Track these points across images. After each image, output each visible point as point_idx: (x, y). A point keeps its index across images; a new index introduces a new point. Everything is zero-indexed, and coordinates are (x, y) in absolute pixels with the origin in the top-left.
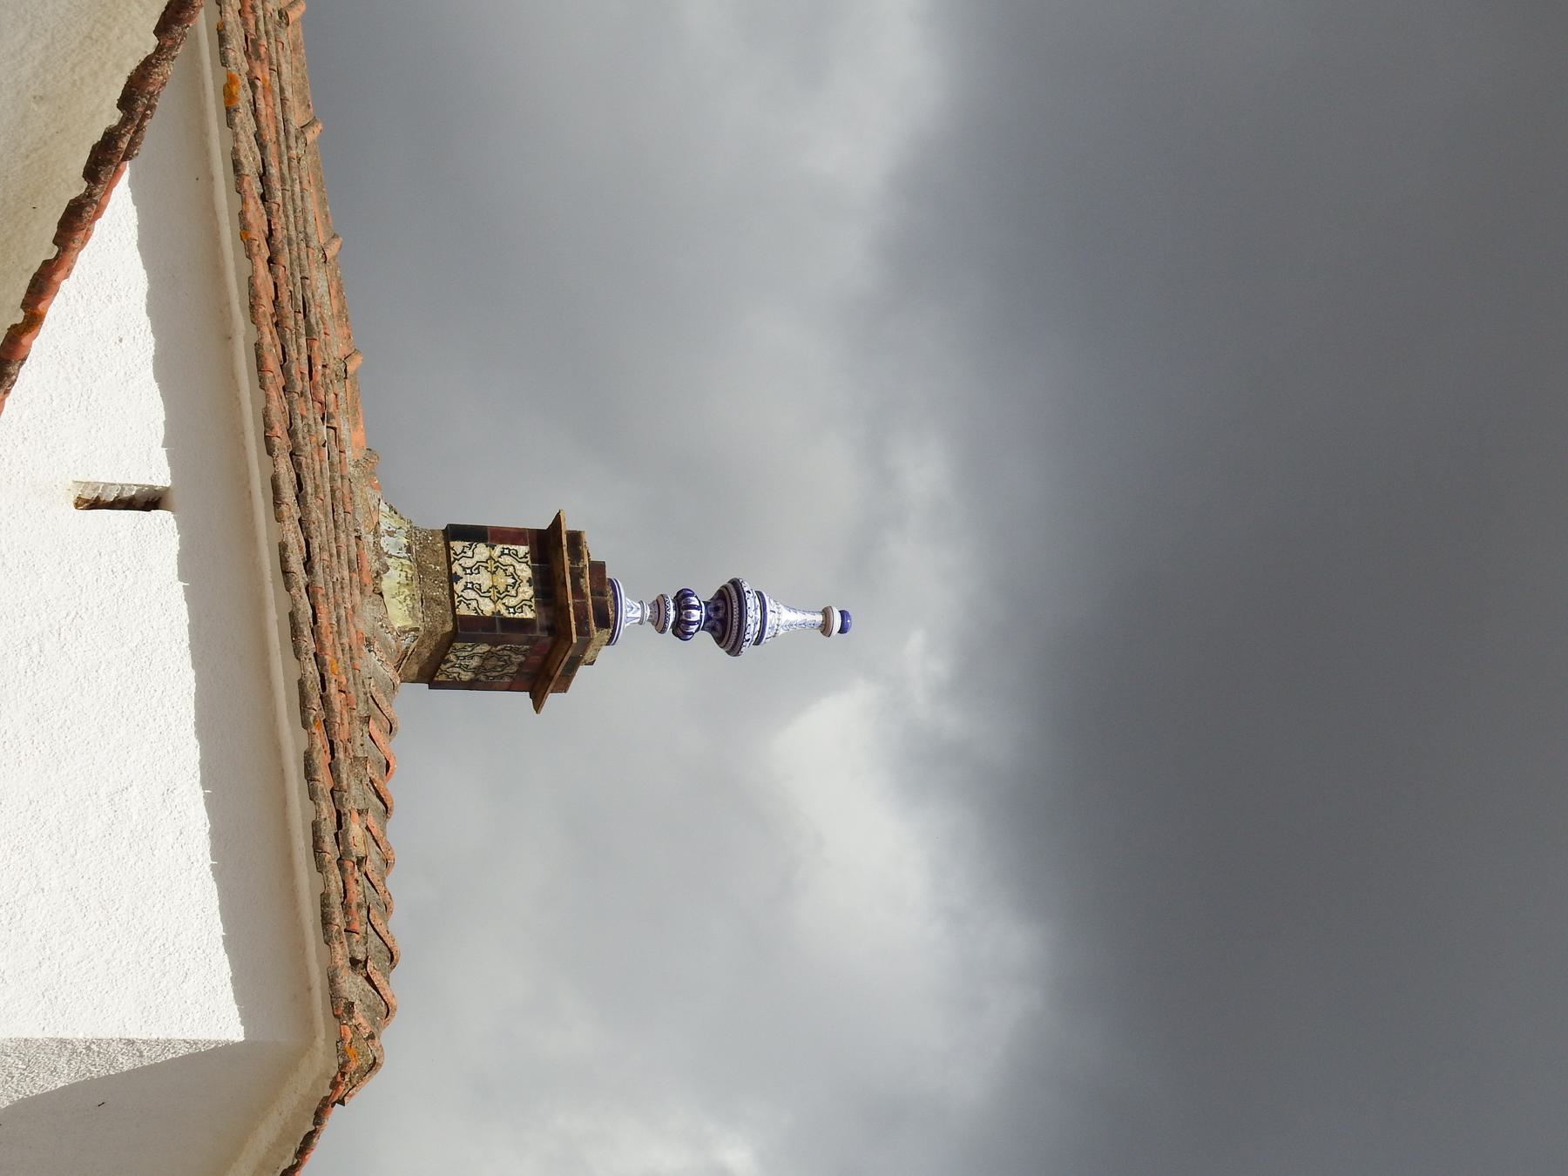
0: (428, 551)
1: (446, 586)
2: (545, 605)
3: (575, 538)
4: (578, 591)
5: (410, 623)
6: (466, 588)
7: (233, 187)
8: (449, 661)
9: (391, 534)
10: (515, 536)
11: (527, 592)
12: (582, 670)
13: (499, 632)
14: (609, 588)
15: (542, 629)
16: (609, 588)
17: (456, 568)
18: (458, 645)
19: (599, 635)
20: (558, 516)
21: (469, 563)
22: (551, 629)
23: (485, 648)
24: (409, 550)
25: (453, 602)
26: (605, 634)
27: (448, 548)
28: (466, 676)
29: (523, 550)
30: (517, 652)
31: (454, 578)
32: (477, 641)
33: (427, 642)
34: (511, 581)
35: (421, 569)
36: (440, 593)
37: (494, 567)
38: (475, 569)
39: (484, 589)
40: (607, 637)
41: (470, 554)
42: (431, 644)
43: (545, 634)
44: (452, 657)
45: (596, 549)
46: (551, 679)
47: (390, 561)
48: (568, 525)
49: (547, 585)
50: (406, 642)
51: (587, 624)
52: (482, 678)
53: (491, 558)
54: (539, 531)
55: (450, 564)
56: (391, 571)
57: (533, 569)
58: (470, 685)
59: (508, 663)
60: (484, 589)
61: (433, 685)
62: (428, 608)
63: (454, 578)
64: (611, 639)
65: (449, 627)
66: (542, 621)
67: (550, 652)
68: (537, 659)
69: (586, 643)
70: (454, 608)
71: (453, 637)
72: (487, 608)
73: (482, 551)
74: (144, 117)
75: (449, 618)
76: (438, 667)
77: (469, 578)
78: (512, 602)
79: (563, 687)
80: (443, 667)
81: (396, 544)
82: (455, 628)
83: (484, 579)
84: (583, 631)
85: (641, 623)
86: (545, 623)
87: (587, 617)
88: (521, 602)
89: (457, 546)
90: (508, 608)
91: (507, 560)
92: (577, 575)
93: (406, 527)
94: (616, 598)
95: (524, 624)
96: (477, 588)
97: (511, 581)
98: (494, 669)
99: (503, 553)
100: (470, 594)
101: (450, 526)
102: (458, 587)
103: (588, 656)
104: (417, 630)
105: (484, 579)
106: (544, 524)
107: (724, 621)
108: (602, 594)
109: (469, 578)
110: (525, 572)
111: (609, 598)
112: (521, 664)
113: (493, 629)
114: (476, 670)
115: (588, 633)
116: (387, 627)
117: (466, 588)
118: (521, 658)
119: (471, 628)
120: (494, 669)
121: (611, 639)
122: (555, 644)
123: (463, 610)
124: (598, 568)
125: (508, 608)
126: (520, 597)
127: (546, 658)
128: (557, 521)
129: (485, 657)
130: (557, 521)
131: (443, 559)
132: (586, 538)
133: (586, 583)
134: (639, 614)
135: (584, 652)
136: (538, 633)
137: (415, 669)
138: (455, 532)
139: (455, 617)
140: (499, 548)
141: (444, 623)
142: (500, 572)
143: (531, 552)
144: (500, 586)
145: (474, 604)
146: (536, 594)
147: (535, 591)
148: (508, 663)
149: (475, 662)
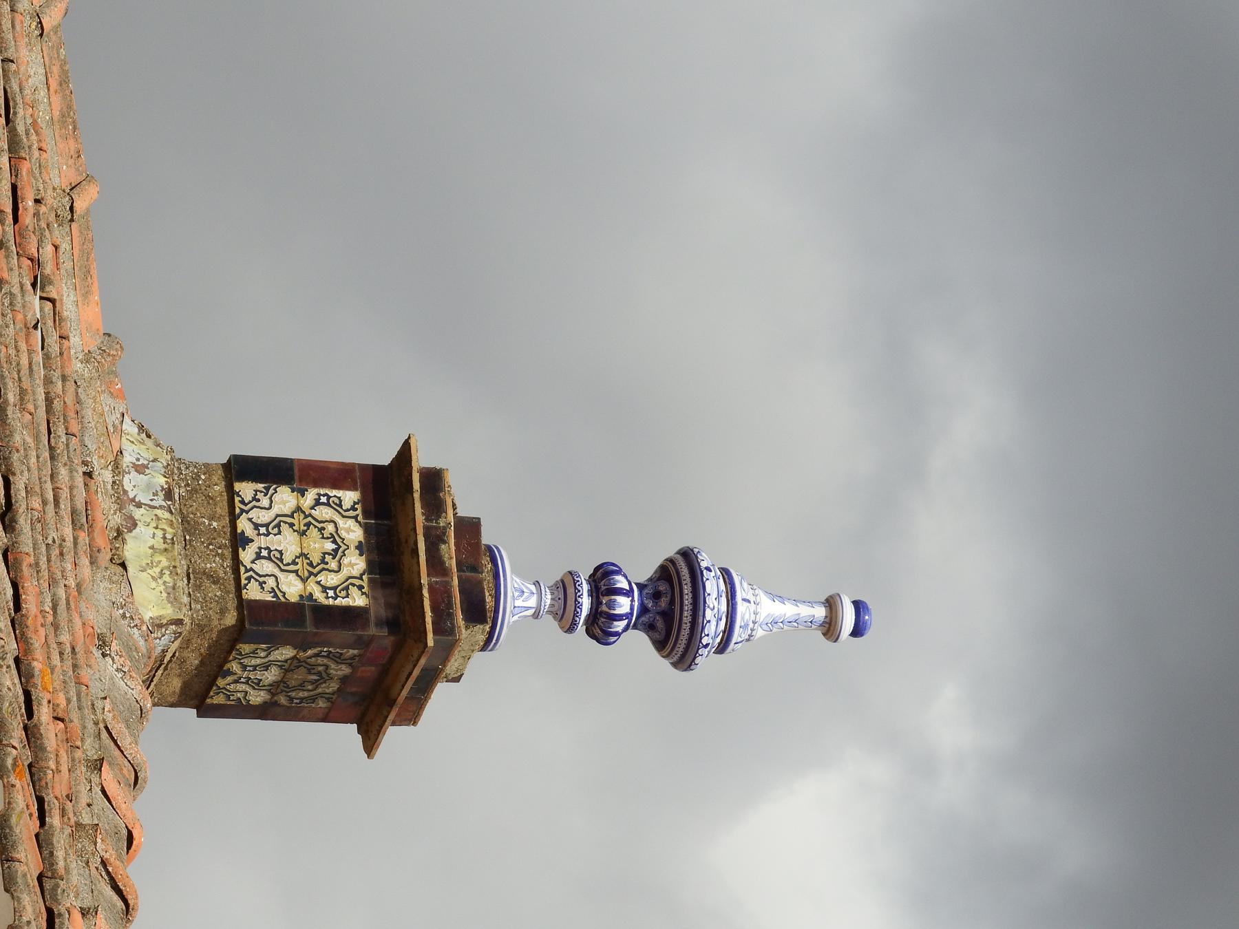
39: (288, 558)
53: (299, 509)
60: (288, 558)
77: (263, 541)
109: (263, 541)
142: (313, 532)
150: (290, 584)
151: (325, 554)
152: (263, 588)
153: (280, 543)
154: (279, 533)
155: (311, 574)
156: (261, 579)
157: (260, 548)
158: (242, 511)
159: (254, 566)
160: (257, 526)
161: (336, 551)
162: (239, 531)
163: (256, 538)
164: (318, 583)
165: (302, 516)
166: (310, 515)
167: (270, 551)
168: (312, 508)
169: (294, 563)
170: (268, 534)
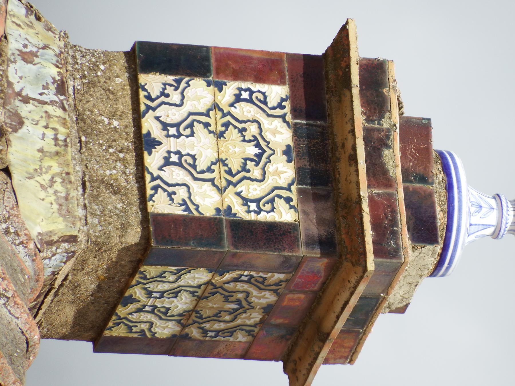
0: (98, 92)
1: (131, 157)
2: (317, 198)
3: (375, 74)
4: (378, 173)
5: (60, 227)
6: (167, 162)
7: (360, 345)
8: (131, 300)
9: (28, 57)
10: (264, 67)
11: (283, 171)
12: (383, 323)
13: (227, 247)
14: (436, 169)
15: (310, 243)
16: (436, 169)
17: (149, 124)
18: (151, 271)
19: (417, 257)
20: (344, 31)
21: (172, 115)
22: (327, 244)
23: (199, 276)
24: (61, 88)
25: (142, 189)
26: (429, 254)
27: (135, 87)
28: (165, 329)
29: (276, 92)
30: (261, 284)
31: (143, 144)
32: (184, 262)
33: (92, 263)
34: (252, 151)
35: (84, 124)
36: (122, 172)
37: (225, 126)
38: (186, 127)
39: (202, 165)
40: (431, 261)
41: (175, 98)
42: (99, 266)
43: (317, 253)
44: (138, 292)
45: (411, 95)
46: (324, 337)
47: (24, 110)
48: (360, 50)
49: (321, 162)
50: (54, 261)
51: (395, 234)
52: (195, 332)
53: (216, 106)
54: (308, 59)
55: (138, 117)
56: (28, 128)
57: (296, 130)
58: (172, 347)
59: (244, 306)
60: (202, 165)
61: (102, 344)
62: (95, 198)
63: (143, 144)
64: (440, 264)
65: (134, 236)
66: (309, 228)
67: (324, 287)
68: (298, 299)
69: (390, 276)
70: (143, 200)
71: (140, 256)
72: (207, 201)
73: (199, 93)
74: (361, 339)
75: (135, 218)
76: (111, 311)
77: (173, 144)
78: (252, 190)
79: (348, 354)
80: (121, 311)
81: (38, 77)
82: (146, 238)
83: (202, 146)
84: (386, 249)
85: (496, 235)
86: (315, 230)
87: (394, 222)
88: (273, 191)
89: (153, 82)
90: (246, 201)
91: (245, 111)
92: (377, 144)
93: (57, 45)
94: (449, 188)
95: (275, 235)
96: (187, 163)
97: (252, 151)
98: (217, 317)
99: (238, 99)
100: (175, 175)
101: (141, 44)
102: (153, 161)
103: (395, 297)
104: (72, 239)
105: (202, 146)
106: (318, 47)
107: (126, 286)
108: (424, 179)
109: (173, 144)
110: (280, 134)
111: (437, 188)
112: (268, 310)
113: (218, 241)
114: (185, 319)
115: (395, 253)
116: (16, 233)
117: (167, 162)
118: (269, 298)
119: (170, 239)
120: (217, 317)
121: (440, 264)
122: (333, 271)
123: (160, 205)
124: (417, 132)
125: (246, 201)
126: (270, 182)
127: (317, 299)
128: (342, 43)
129: (201, 294)
130: (342, 43)
131: (125, 105)
132: (396, 73)
133: (393, 158)
134: (492, 219)
135: (388, 287)
136: (302, 251)
137: (69, 312)
138: (148, 57)
139: (146, 218)
140: (231, 88)
141: (124, 227)
142: (232, 134)
143: (293, 96)
144: (229, 158)
145: (181, 193)
146: (301, 176)
147: (299, 171)
148: (244, 306)
149: (182, 304)
150: (204, 196)
151: (246, 159)
152: (172, 200)
153: (193, 146)
154: (192, 134)
155: (229, 183)
156: (170, 189)
157: (169, 152)
158: (148, 108)
159: (162, 174)
160: (165, 126)
161: (259, 156)
162: (144, 131)
163: (164, 140)
164: (238, 194)
165: (219, 114)
166: (229, 114)
167: (181, 156)
168: (232, 105)
169: (209, 170)
170: (179, 135)
